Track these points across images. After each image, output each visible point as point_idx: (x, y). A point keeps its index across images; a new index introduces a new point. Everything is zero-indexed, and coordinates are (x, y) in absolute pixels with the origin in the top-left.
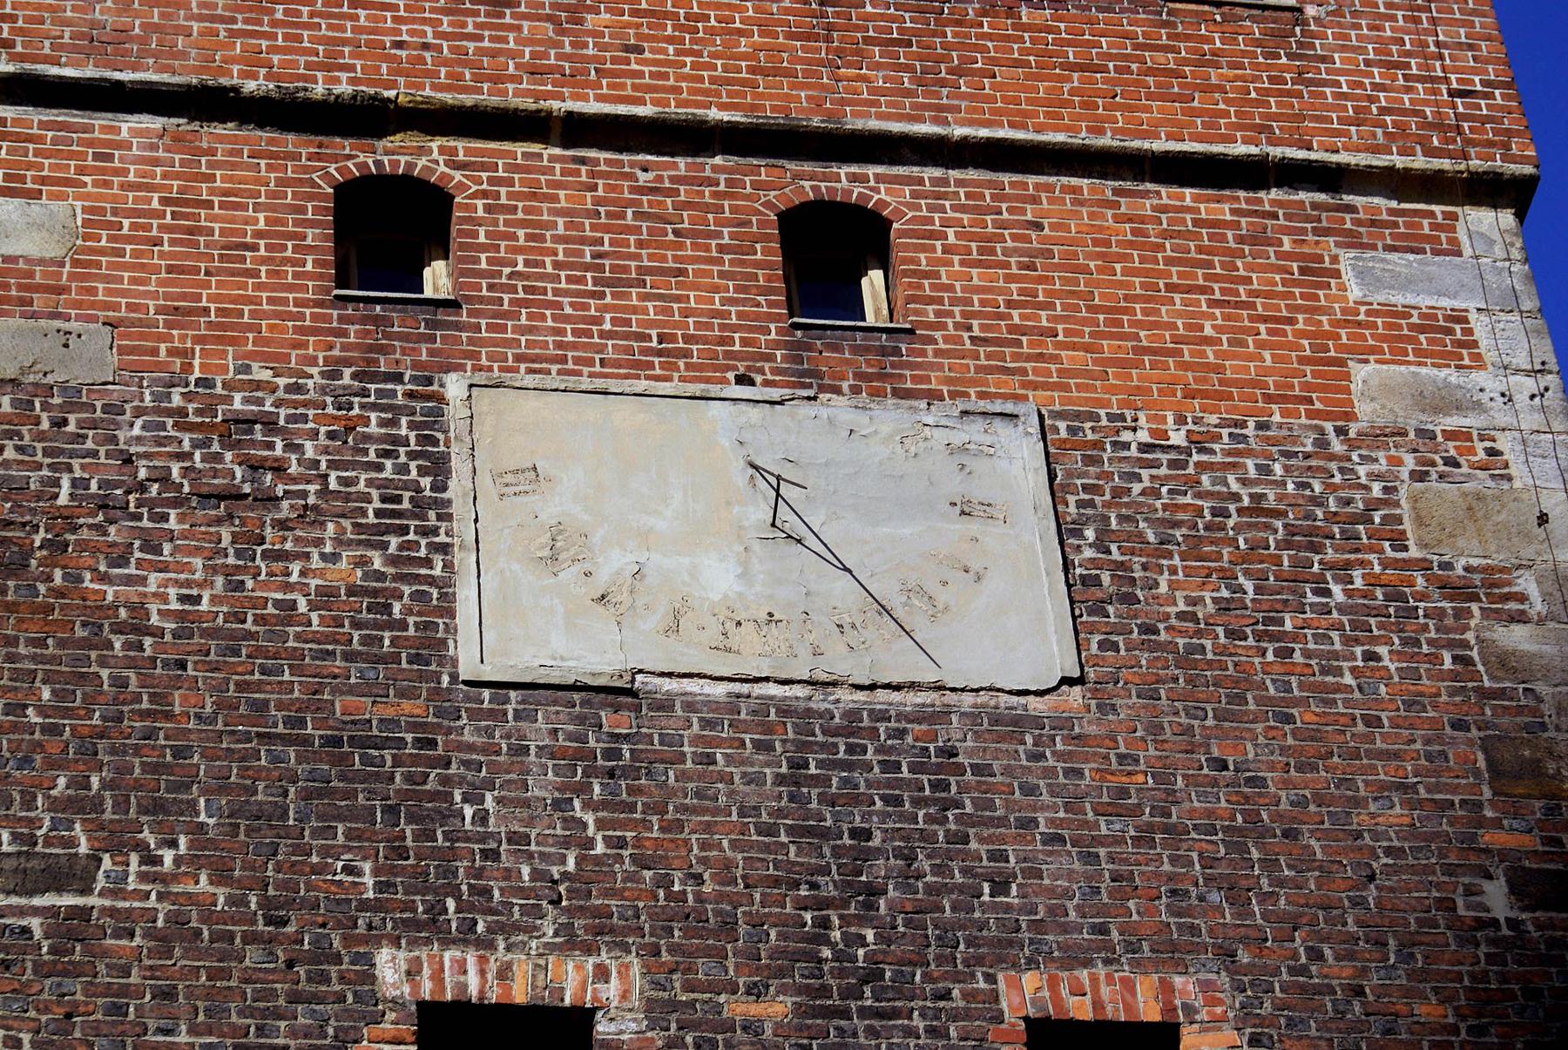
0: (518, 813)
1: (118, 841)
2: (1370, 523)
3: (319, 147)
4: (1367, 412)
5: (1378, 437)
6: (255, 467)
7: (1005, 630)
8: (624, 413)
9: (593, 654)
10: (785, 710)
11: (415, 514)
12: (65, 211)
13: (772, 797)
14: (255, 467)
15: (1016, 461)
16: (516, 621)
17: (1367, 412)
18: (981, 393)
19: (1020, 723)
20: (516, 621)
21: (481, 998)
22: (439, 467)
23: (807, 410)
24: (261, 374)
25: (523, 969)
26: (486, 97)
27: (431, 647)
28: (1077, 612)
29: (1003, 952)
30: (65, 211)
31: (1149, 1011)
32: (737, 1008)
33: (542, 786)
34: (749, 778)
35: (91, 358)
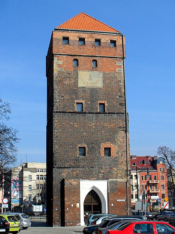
0: (81, 94)
1: (65, 95)
2: (116, 78)
3: (141, 190)
4: (116, 71)
5: (117, 73)
6: (70, 76)
7: (99, 84)
8: (85, 72)
9: (84, 86)
10: (91, 88)
11: (77, 78)
12: (62, 61)
13: (90, 92)
14: (70, 76)
15: (101, 75)
16: (81, 84)
17: (116, 71)
18: (100, 71)
19: (100, 89)
20: (81, 84)
21: (54, 120)
22: (78, 76)
23: (92, 72)
24: (70, 71)
25: (80, 101)
26: (80, 55)
27: (77, 85)
28: (77, 109)
29: (98, 100)
30: (62, 61)
31: (104, 103)
32: (88, 103)
33: (81, 92)
34: (89, 92)
35: (63, 70)
